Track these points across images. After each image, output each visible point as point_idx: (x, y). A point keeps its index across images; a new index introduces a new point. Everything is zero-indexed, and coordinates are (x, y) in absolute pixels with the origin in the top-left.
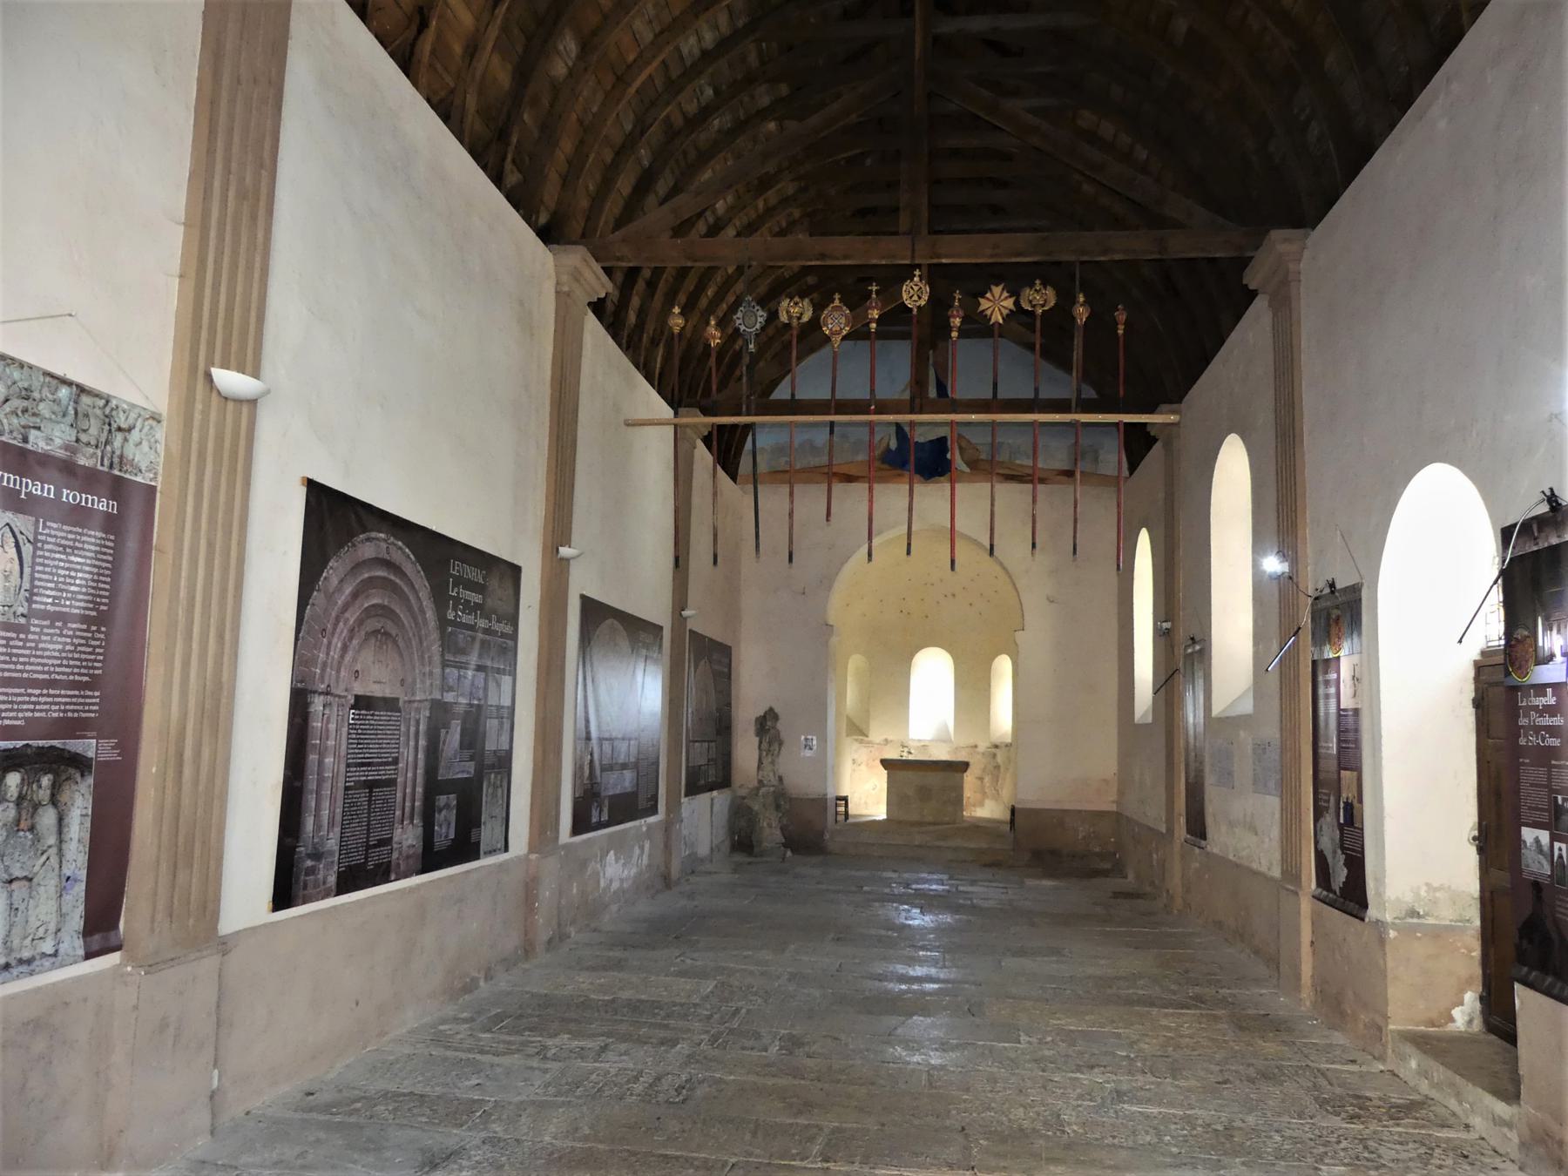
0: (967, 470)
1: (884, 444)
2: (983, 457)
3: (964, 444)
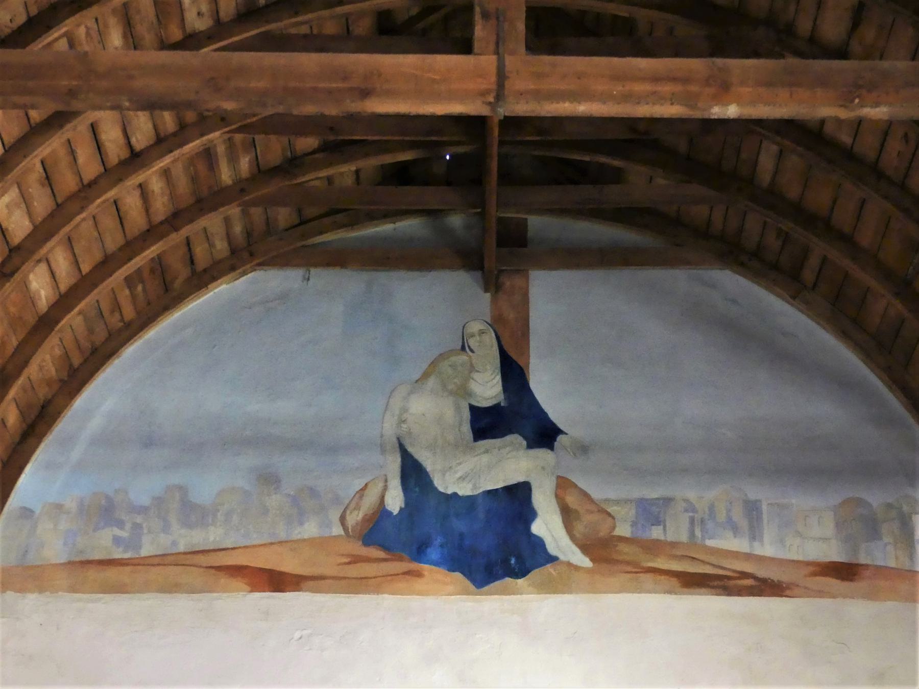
0: (584, 562)
1: (369, 502)
2: (623, 530)
3: (572, 500)
